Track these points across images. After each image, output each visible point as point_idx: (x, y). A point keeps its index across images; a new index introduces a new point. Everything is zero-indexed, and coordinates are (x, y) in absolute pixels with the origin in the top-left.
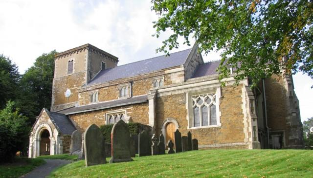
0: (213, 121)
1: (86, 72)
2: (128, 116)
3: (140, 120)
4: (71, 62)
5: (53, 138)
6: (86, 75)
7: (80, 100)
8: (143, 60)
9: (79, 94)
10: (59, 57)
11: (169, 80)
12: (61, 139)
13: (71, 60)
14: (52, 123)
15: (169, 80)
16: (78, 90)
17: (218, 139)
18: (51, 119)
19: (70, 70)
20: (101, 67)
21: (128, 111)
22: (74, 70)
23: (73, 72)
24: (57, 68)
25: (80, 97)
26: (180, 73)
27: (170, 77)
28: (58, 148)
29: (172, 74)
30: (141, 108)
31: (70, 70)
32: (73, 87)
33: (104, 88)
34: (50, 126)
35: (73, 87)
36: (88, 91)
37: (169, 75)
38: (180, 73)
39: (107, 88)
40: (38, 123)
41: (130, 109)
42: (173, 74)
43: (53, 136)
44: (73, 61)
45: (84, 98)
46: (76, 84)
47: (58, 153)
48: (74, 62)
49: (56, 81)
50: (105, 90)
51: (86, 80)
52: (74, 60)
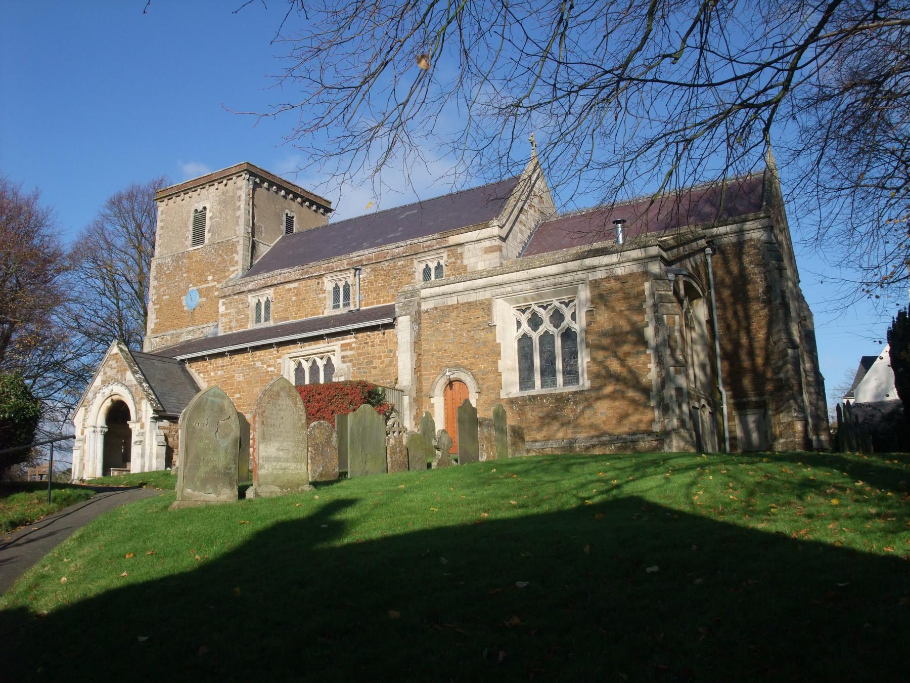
0: (571, 374)
1: (241, 242)
2: (344, 362)
3: (373, 372)
4: (200, 218)
5: (138, 425)
6: (240, 248)
7: (224, 320)
8: (800, 276)
9: (221, 301)
10: (169, 197)
11: (459, 261)
12: (159, 428)
13: (200, 209)
14: (135, 382)
15: (459, 261)
16: (218, 289)
17: (646, 320)
18: (134, 372)
19: (198, 237)
20: (283, 227)
21: (344, 347)
22: (207, 236)
23: (206, 241)
24: (162, 228)
25: (222, 309)
26: (487, 244)
27: (461, 254)
28: (151, 453)
29: (466, 247)
30: (377, 336)
31: (198, 237)
32: (206, 281)
33: (287, 286)
34: (131, 392)
35: (206, 281)
36: (243, 292)
37: (459, 250)
38: (487, 244)
39: (296, 285)
40: (98, 381)
41: (349, 344)
42: (471, 246)
43: (139, 420)
44: (205, 208)
45: (233, 311)
46: (214, 275)
47: (150, 466)
48: (209, 215)
49: (160, 266)
50: (290, 290)
51: (240, 263)
52: (208, 207)
